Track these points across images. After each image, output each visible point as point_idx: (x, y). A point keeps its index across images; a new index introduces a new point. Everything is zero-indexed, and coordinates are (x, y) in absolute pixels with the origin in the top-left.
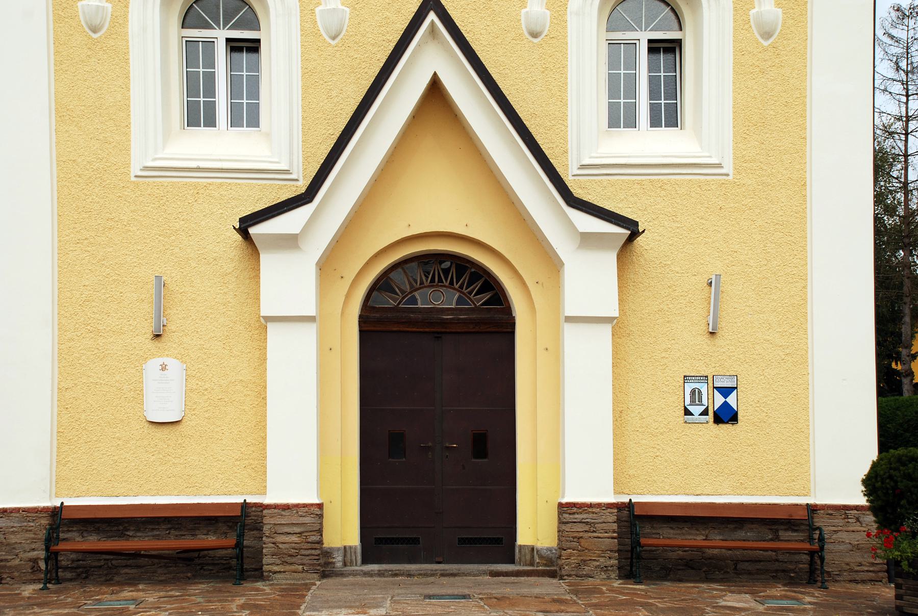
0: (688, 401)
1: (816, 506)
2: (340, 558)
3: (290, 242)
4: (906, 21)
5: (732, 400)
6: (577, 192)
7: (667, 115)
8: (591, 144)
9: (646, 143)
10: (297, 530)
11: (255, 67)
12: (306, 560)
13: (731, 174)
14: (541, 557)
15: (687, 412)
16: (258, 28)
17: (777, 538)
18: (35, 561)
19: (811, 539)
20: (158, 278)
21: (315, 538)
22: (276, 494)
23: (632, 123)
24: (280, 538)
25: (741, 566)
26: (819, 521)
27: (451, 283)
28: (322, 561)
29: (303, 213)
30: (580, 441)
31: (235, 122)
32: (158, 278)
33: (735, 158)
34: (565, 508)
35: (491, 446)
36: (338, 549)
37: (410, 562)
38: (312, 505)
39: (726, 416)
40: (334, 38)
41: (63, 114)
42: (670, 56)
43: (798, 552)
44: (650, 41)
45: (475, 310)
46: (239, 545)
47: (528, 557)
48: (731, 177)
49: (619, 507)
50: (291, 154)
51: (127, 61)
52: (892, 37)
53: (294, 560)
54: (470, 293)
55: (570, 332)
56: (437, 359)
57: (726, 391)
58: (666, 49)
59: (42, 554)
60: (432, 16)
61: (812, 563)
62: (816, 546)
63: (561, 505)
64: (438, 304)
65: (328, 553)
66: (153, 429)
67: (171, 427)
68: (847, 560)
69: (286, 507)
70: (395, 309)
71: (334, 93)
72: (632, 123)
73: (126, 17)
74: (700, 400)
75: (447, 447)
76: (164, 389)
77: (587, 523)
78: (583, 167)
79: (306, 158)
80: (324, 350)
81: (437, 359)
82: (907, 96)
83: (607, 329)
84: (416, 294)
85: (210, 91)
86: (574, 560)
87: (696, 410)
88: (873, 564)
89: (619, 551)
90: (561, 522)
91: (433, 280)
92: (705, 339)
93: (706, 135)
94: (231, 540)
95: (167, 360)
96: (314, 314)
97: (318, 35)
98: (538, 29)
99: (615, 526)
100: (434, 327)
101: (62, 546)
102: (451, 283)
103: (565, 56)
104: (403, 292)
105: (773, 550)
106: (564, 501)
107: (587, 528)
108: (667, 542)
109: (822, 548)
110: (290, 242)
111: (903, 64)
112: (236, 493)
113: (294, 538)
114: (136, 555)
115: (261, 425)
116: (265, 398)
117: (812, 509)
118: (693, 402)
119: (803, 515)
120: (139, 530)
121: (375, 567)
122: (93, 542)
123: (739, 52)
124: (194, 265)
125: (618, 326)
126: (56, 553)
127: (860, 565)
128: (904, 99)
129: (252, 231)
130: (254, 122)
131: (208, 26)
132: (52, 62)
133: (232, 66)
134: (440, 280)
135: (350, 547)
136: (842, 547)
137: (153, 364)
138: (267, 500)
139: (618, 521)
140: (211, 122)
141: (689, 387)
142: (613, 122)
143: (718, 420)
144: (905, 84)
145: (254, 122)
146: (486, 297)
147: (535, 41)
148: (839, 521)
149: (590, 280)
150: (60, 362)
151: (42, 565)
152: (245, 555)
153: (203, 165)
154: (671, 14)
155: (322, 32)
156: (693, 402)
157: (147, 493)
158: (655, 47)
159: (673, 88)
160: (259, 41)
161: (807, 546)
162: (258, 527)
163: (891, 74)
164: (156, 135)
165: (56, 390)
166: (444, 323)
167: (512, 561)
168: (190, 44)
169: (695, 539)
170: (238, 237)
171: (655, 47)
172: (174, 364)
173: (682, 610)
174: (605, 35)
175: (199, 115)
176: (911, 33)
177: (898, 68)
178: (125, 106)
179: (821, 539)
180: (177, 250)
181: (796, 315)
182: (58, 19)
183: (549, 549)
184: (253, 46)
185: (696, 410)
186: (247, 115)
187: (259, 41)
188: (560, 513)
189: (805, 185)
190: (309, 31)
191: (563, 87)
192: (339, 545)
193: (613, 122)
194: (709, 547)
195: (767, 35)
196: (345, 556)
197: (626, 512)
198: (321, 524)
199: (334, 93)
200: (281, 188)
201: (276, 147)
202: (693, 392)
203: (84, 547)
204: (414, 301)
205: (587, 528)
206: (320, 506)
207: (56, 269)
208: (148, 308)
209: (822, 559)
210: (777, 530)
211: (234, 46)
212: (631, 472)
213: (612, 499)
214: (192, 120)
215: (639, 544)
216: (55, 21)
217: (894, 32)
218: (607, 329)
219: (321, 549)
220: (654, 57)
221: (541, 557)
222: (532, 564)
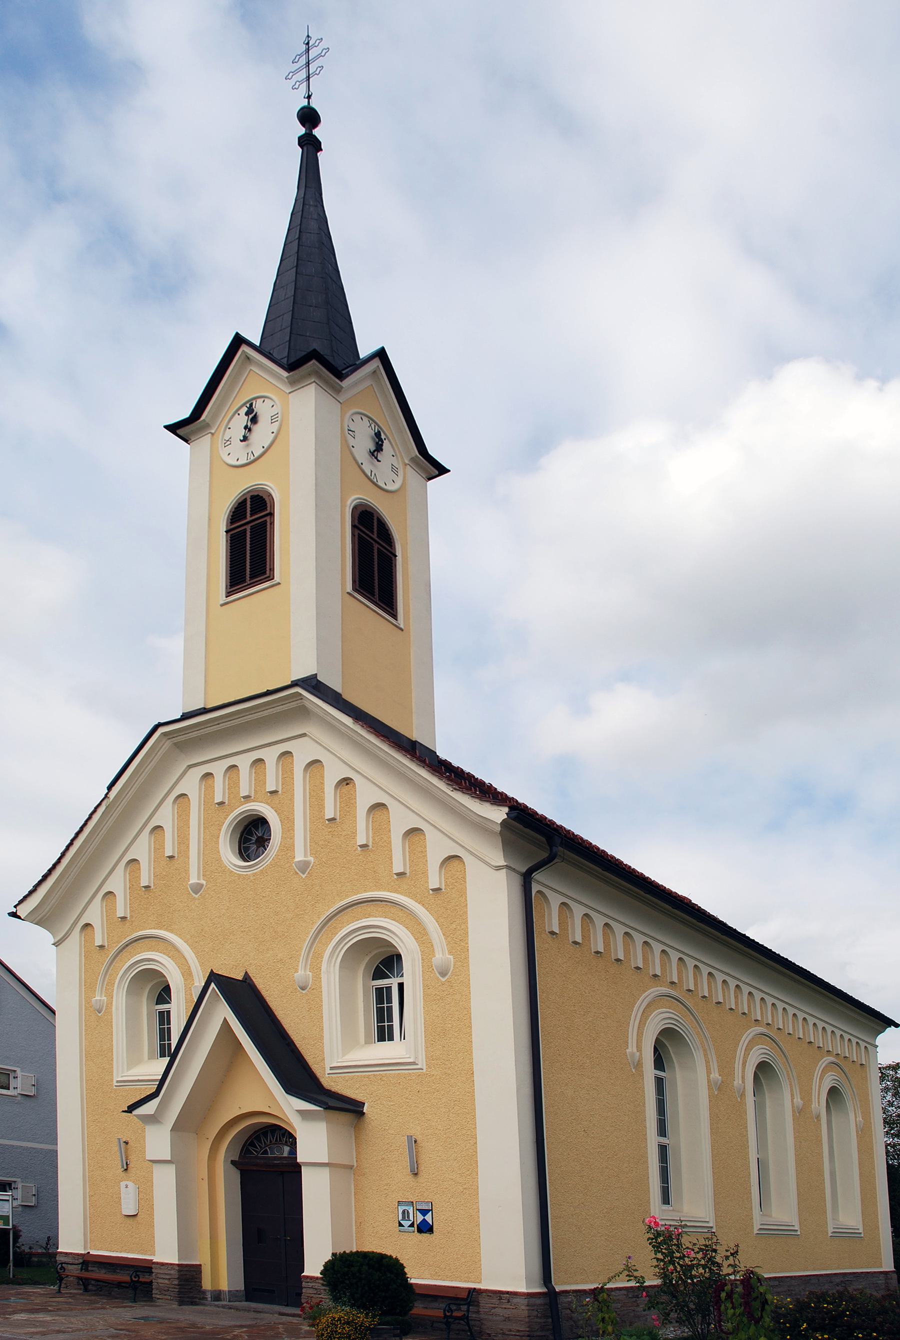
0: (400, 1218)
1: (480, 1290)
5: (428, 1218)
10: (168, 1277)
13: (424, 1068)
15: (400, 1225)
24: (160, 1281)
25: (435, 1325)
29: (155, 1102)
39: (425, 1228)
57: (424, 1212)
68: (501, 1327)
74: (408, 1217)
87: (406, 1223)
88: (519, 1331)
92: (410, 1178)
110: (152, 1119)
118: (404, 1218)
119: (464, 1295)
121: (253, 1305)
136: (498, 1318)
137: (123, 1184)
141: (401, 1209)
143: (420, 1230)
148: (495, 1301)
168: (379, 991)
173: (117, 1336)
181: (470, 1162)
185: (406, 1223)
195: (443, 974)
202: (404, 1212)
204: (266, 1152)
214: (381, 1038)
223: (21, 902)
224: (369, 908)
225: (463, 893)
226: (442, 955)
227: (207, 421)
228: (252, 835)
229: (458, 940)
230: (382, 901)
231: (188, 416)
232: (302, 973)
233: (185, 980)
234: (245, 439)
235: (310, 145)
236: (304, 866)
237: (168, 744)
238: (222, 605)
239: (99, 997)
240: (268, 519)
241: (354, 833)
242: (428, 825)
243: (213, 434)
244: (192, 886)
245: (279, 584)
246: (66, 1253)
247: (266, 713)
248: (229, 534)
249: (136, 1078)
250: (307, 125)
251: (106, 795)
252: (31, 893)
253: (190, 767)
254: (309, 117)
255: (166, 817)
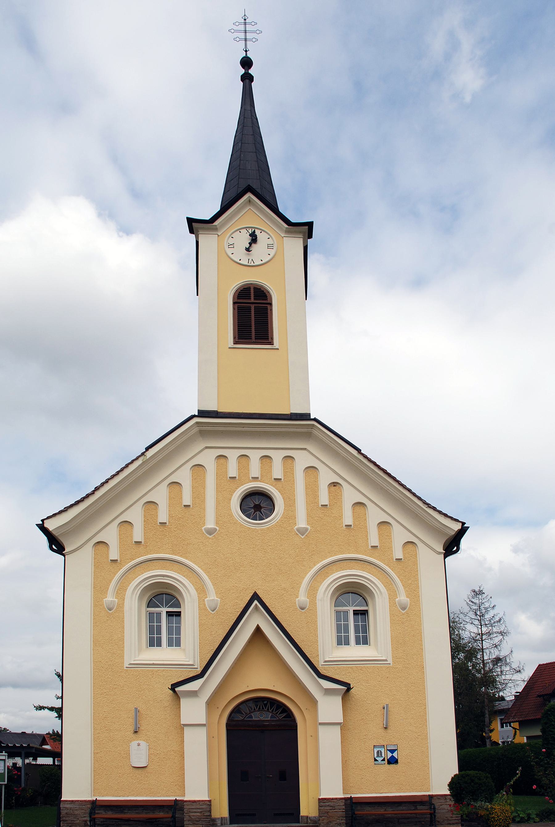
0: (376, 755)
2: (219, 822)
3: (194, 694)
4: (478, 596)
5: (395, 754)
6: (323, 672)
7: (363, 639)
8: (329, 651)
9: (354, 652)
11: (179, 622)
12: (204, 823)
14: (311, 820)
15: (375, 760)
16: (179, 606)
17: (416, 809)
18: (86, 821)
19: (431, 808)
20: (136, 709)
21: (209, 814)
22: (188, 797)
23: (347, 643)
26: (434, 801)
27: (268, 709)
28: (211, 823)
30: (326, 771)
31: (170, 644)
32: (136, 709)
33: (393, 657)
34: (321, 800)
35: (287, 775)
36: (219, 818)
37: (252, 823)
38: (206, 801)
39: (393, 761)
40: (213, 611)
41: (96, 643)
42: (363, 616)
43: (426, 814)
44: (354, 611)
45: (279, 720)
46: (173, 817)
47: (305, 820)
48: (391, 665)
49: (345, 799)
50: (194, 657)
51: (123, 622)
52: (473, 602)
53: (198, 823)
54: (277, 713)
55: (321, 729)
56: (261, 740)
57: (392, 751)
58: (362, 614)
59: (88, 819)
60: (256, 602)
61: (431, 818)
62: (432, 811)
63: (320, 800)
64: (262, 718)
65: (214, 820)
66: (135, 770)
67: (140, 770)
68: (447, 816)
69: (194, 802)
70: (243, 720)
71: (213, 633)
72: (347, 643)
73: (123, 604)
74: (381, 755)
75: (268, 777)
76: (139, 753)
77: (331, 806)
78: (326, 661)
79: (201, 659)
80: (210, 738)
81: (261, 740)
82: (481, 625)
83: (338, 728)
84: (252, 714)
85: (159, 632)
86: (325, 821)
87: (380, 759)
89: (346, 817)
90: (320, 806)
91: (259, 708)
92: (382, 731)
93: (380, 647)
94: (170, 815)
95: (140, 742)
96: (205, 723)
97: (206, 609)
98: (304, 606)
99: (344, 807)
100: (261, 728)
101: (96, 816)
102: (268, 709)
103: (316, 616)
104: (246, 714)
105: (414, 813)
106: (320, 797)
107: (331, 808)
108: (368, 812)
109: (435, 812)
110: (194, 694)
111: (478, 613)
112: (172, 796)
113: (198, 814)
114: (128, 820)
115: (182, 768)
116: (184, 757)
117: (431, 797)
118: (378, 756)
119: (427, 799)
120: (129, 810)
122: (110, 814)
123: (392, 615)
124: (151, 703)
125: (343, 726)
126: (94, 819)
127: (452, 817)
128: (480, 627)
129: (176, 689)
130: (178, 644)
131: (159, 607)
132: (92, 622)
133: (168, 622)
134: (263, 708)
135: (224, 818)
137: (134, 744)
138: (185, 799)
139: (345, 804)
140: (159, 645)
142: (339, 643)
143: (389, 762)
144: (480, 621)
145: (178, 644)
146: (285, 715)
147: (303, 611)
148: (443, 801)
149: (330, 708)
150: (94, 742)
151: (89, 823)
152: (176, 820)
153: (155, 662)
154: (363, 600)
155: (208, 608)
156: (378, 756)
157: (133, 795)
158: (356, 613)
159: (365, 629)
160: (180, 612)
161: (429, 811)
162: (182, 809)
163: (474, 617)
164: (137, 651)
165: (93, 754)
166: (265, 726)
167: (299, 822)
168: (151, 614)
169: (381, 811)
170: (171, 692)
171: (356, 613)
172: (143, 744)
174: (334, 608)
175: (154, 642)
176: (480, 600)
177: (476, 615)
178: (122, 640)
179: (434, 808)
180: (144, 697)
181: (422, 719)
182: (95, 606)
183: (315, 817)
184: (178, 614)
186: (175, 641)
187: (180, 612)
188: (319, 803)
189: (423, 667)
190: (202, 608)
191: (316, 629)
192: (219, 817)
193: (339, 643)
194: (387, 814)
195: (404, 608)
196: (222, 821)
197: (349, 801)
198: (210, 808)
199: (213, 633)
200: (190, 671)
201: (186, 655)
202: (378, 752)
203: (106, 816)
205: (331, 808)
206: (210, 801)
207: (92, 705)
208: (131, 721)
209: (435, 816)
210: (416, 806)
211: (169, 614)
212: (351, 785)
213: (342, 796)
215: (354, 814)
216: (94, 607)
217: (473, 600)
218: (338, 728)
219: (211, 818)
220: (357, 616)
221: (311, 820)
222: (307, 823)
223: (48, 518)
224: (353, 563)
225: (415, 563)
226: (403, 597)
227: (218, 227)
228: (257, 504)
229: (414, 590)
230: (361, 561)
231: (208, 219)
232: (302, 598)
233: (199, 594)
234: (248, 250)
235: (247, 79)
236: (302, 531)
237: (196, 429)
238: (230, 348)
239: (110, 598)
240: (236, 301)
241: (341, 517)
242: (120, 517)
243: (218, 236)
244: (298, 530)
245: (278, 349)
246: (72, 801)
247: (283, 430)
248: (236, 305)
249: (151, 662)
250: (246, 67)
251: (143, 454)
252: (60, 512)
253: (207, 448)
254: (246, 63)
255: (184, 477)
